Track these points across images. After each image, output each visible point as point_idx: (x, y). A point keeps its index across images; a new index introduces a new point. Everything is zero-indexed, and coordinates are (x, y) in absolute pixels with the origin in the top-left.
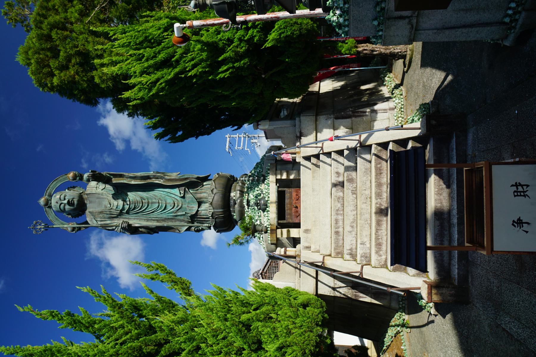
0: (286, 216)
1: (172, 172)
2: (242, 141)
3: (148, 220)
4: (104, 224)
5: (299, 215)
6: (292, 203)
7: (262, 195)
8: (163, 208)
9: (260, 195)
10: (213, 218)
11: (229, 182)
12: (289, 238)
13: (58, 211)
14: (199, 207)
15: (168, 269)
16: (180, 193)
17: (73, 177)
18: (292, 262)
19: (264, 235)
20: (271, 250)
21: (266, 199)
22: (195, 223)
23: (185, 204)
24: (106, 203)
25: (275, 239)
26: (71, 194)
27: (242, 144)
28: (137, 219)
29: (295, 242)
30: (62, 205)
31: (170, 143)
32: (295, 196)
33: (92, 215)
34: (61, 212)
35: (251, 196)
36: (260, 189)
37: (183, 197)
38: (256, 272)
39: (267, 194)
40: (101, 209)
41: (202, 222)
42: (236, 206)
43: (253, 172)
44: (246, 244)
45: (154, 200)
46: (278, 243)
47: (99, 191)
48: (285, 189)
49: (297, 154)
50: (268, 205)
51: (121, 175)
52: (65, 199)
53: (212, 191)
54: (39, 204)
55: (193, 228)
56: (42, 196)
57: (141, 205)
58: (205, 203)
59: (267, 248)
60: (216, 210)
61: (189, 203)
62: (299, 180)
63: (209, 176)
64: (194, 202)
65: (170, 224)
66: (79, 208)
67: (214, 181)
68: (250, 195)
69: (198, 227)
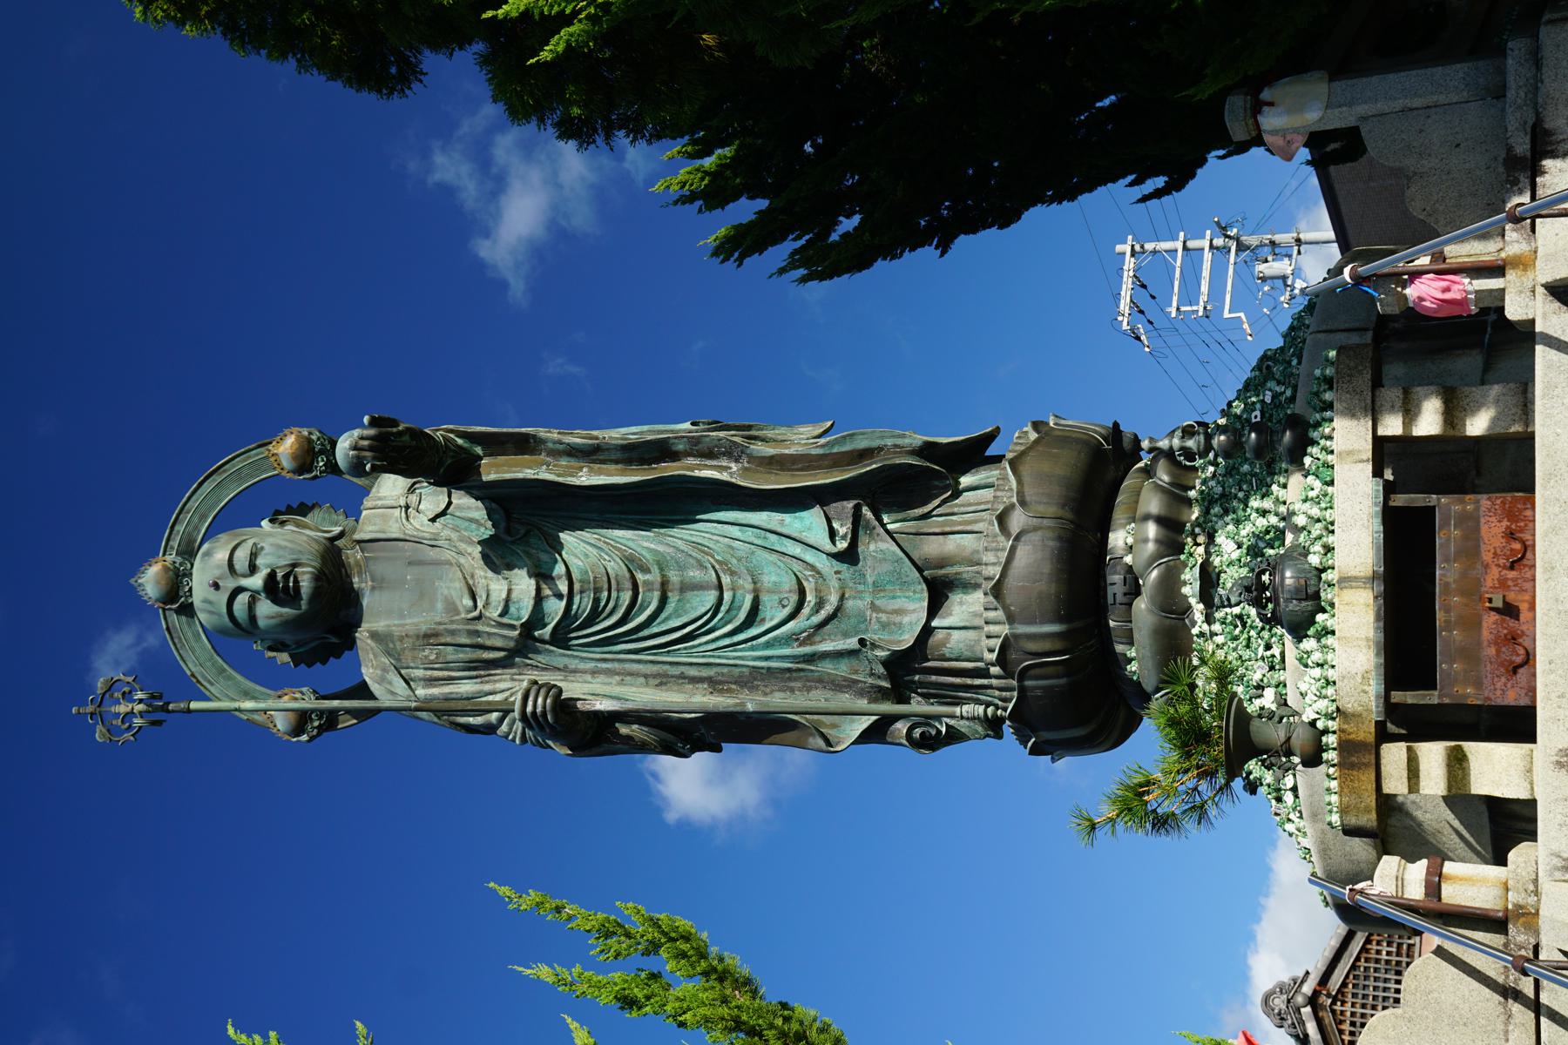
0: (1442, 666)
1: (790, 424)
2: (1206, 273)
3: (663, 681)
4: (447, 699)
5: (1529, 659)
6: (1478, 583)
7: (1289, 537)
8: (742, 616)
9: (1281, 534)
10: (1008, 674)
11: (1099, 472)
12: (1458, 798)
13: (222, 631)
14: (933, 611)
15: (714, 950)
16: (832, 534)
17: (295, 457)
18: (1480, 949)
19: (1304, 778)
20: (1346, 867)
21: (1314, 560)
22: (916, 699)
23: (859, 595)
24: (451, 587)
25: (1371, 801)
26: (281, 544)
27: (1204, 288)
28: (610, 673)
29: (1504, 825)
30: (243, 598)
31: (804, 280)
32: (1499, 542)
33: (388, 653)
34: (236, 634)
35: (1228, 548)
36: (1277, 501)
37: (849, 556)
38: (1281, 988)
39: (1317, 530)
40: (420, 621)
41: (950, 695)
42: (1142, 605)
43: (1238, 407)
44: (1189, 824)
45: (694, 574)
46: (1390, 828)
47: (420, 524)
48: (1433, 499)
49: (1511, 275)
50: (1326, 595)
51: (526, 436)
52: (253, 569)
53: (1002, 519)
54: (133, 593)
55: (901, 727)
56: (149, 555)
57: (626, 597)
58: (969, 586)
59: (1324, 852)
61: (878, 588)
62: (1526, 442)
63: (990, 438)
64: (904, 585)
65: (778, 700)
66: (322, 617)
67: (1012, 463)
68: (1220, 539)
69: (928, 718)
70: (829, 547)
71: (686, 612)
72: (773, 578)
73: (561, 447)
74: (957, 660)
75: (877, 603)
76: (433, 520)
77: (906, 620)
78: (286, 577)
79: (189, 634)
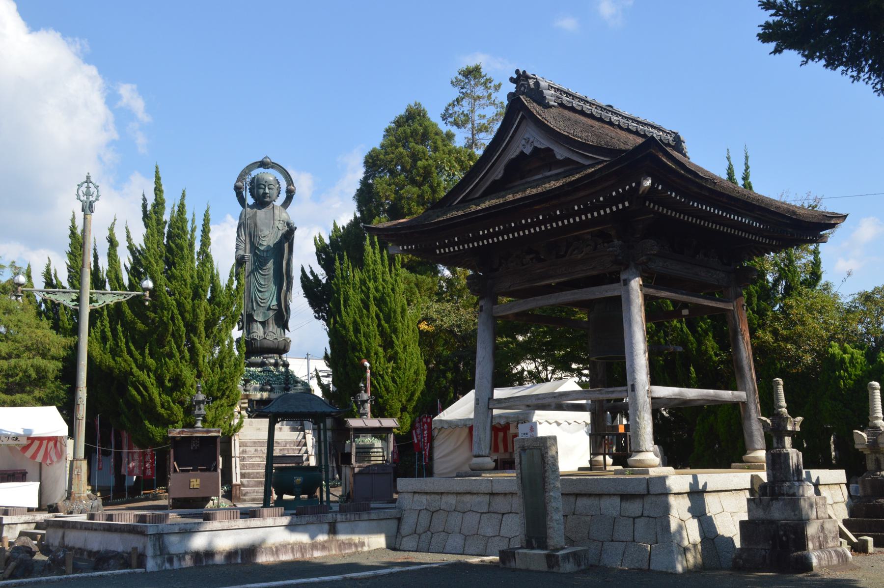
14: (260, 323)
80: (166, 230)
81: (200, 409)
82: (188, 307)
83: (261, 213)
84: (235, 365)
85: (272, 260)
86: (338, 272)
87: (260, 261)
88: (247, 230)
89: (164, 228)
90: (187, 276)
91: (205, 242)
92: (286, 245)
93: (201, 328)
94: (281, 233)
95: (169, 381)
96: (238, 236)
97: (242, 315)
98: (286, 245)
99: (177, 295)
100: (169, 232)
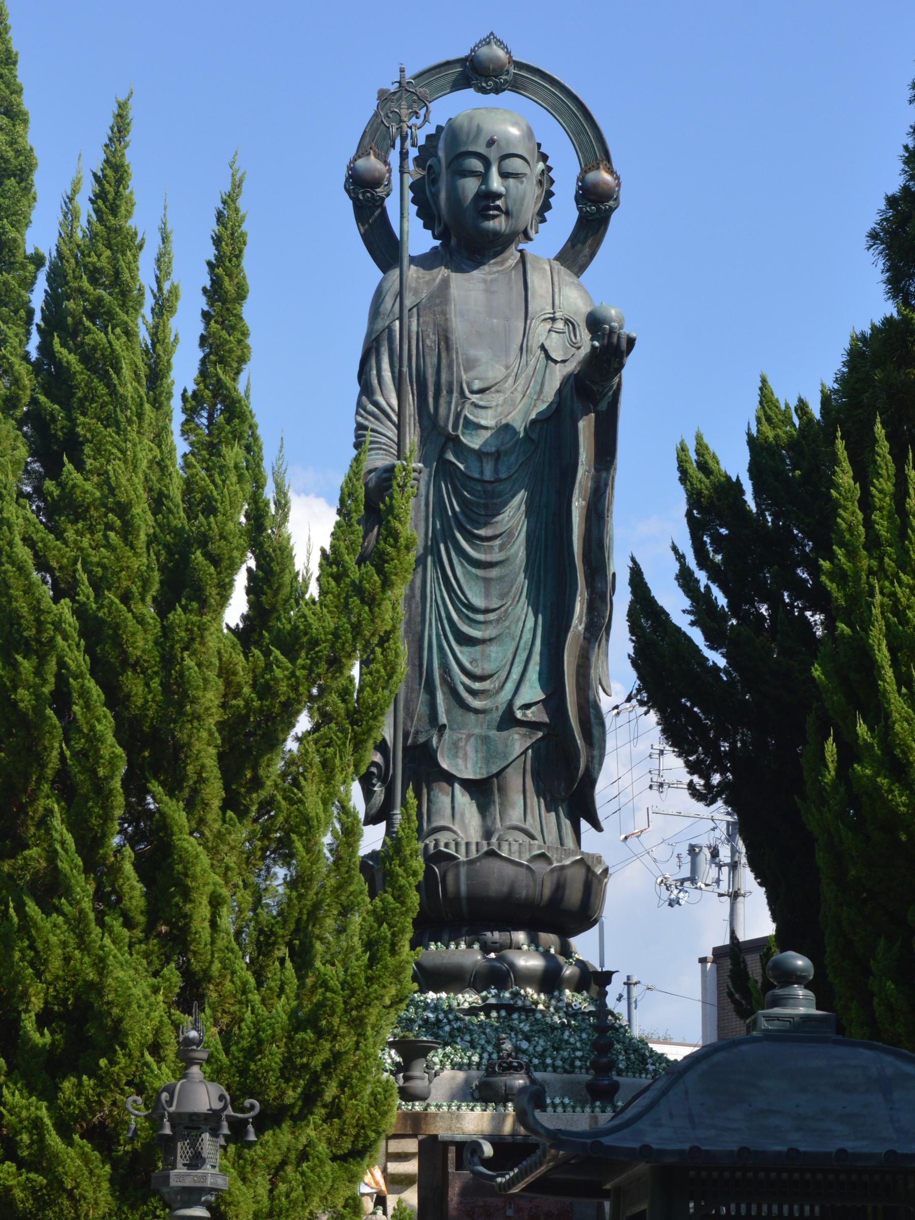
8: (477, 686)
14: (467, 784)
16: (527, 706)
30: (477, 165)
33: (431, 297)
52: (504, 175)
60: (463, 871)
70: (519, 702)
71: (467, 581)
72: (493, 655)
73: (602, 484)
74: (429, 800)
75: (472, 739)
76: (542, 347)
77: (460, 762)
78: (498, 208)
79: (442, 82)
80: (37, 298)
81: (196, 1161)
82: (141, 643)
83: (469, 290)
84: (369, 945)
85: (521, 496)
86: (850, 515)
87: (467, 501)
88: (406, 364)
89: (28, 284)
90: (134, 490)
91: (223, 347)
92: (585, 426)
93: (206, 753)
94: (556, 376)
95: (43, 1020)
96: (366, 389)
97: (382, 747)
98: (585, 426)
99: (86, 590)
100: (53, 301)
